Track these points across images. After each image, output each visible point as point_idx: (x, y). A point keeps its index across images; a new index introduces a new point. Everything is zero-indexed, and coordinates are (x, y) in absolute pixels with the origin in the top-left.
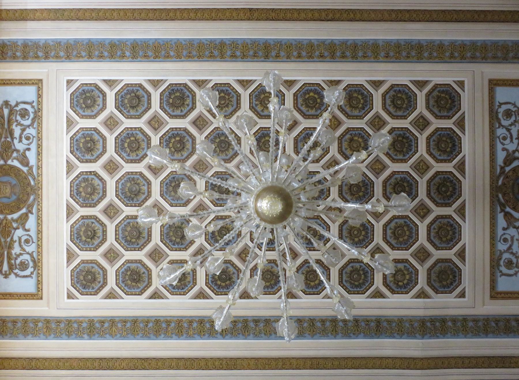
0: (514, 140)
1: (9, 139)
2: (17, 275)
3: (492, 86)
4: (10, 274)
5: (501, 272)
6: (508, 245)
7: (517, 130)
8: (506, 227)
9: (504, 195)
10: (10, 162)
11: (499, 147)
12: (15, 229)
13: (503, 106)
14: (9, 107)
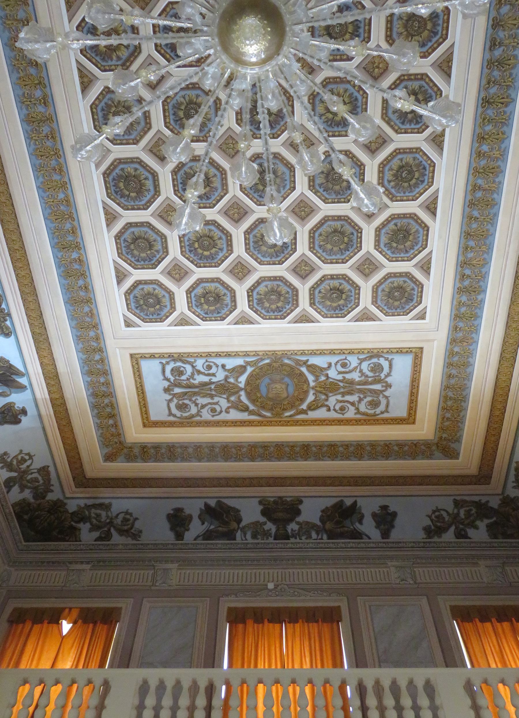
1: (213, 387)
2: (389, 375)
8: (227, 368)
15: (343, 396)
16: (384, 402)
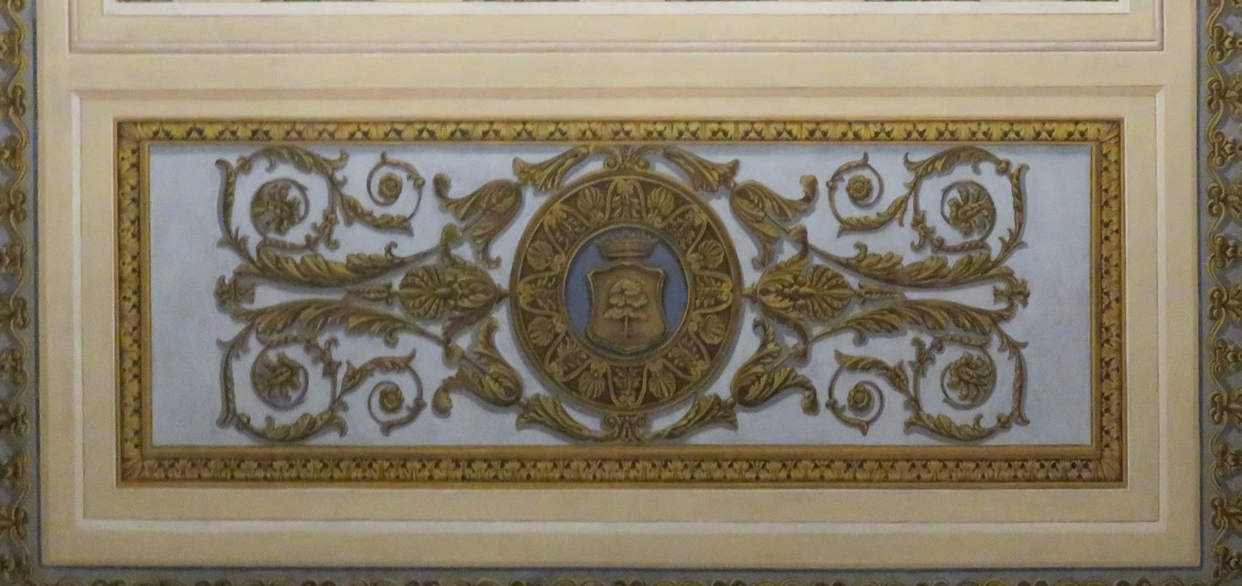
1: (396, 281)
2: (1013, 243)
4: (1008, 276)
10: (501, 278)
11: (822, 164)
15: (861, 341)
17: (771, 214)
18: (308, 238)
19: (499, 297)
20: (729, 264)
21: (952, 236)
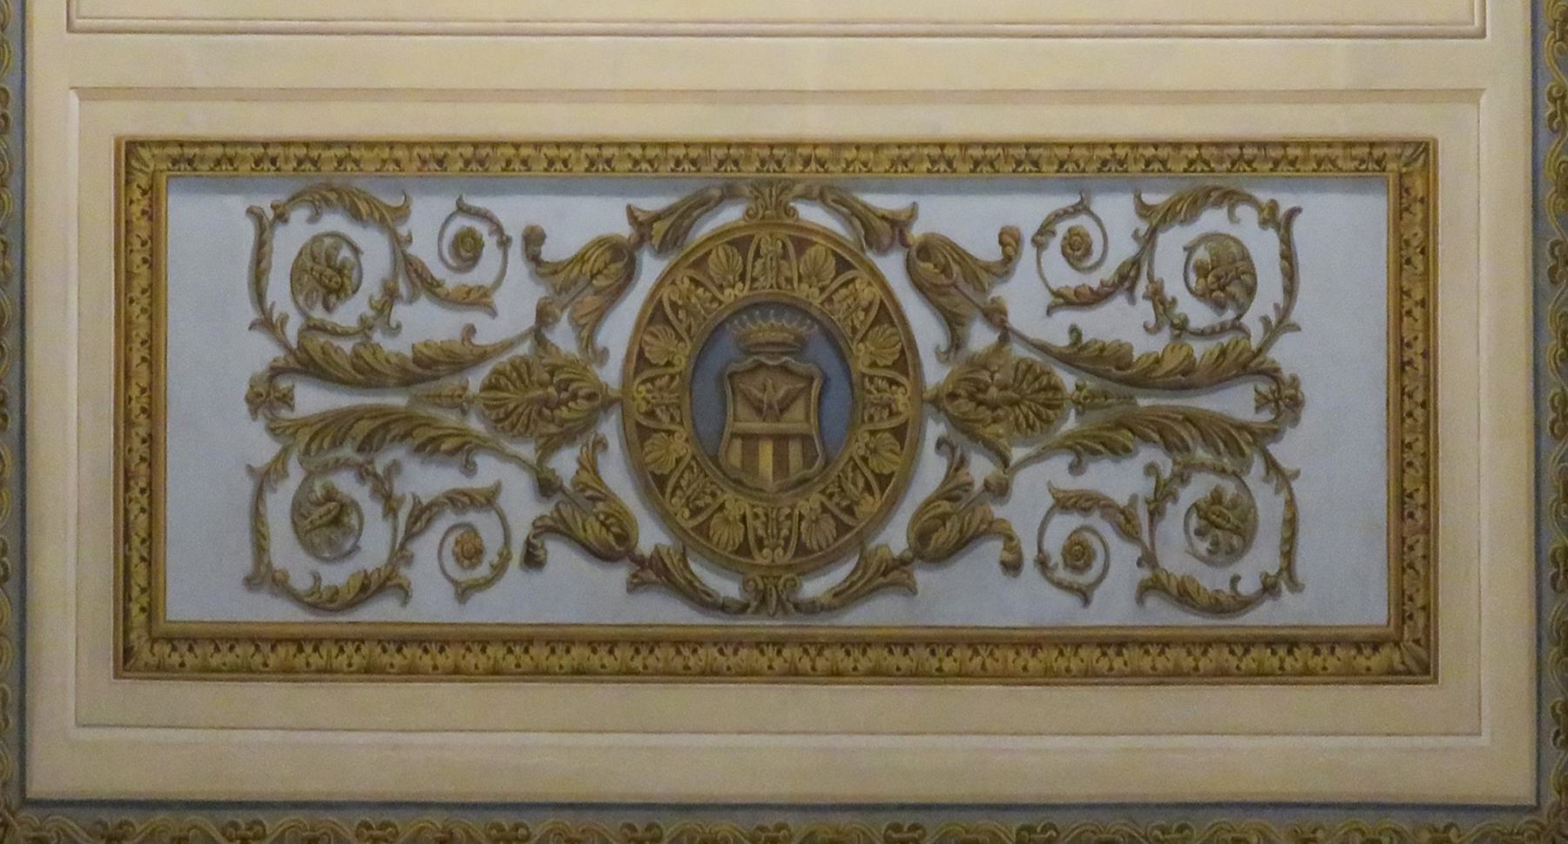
0: (1066, 317)
1: (475, 380)
2: (1281, 324)
3: (1392, 166)
4: (1272, 374)
5: (281, 217)
6: (438, 271)
7: (1125, 338)
8: (549, 253)
9: (738, 242)
10: (610, 374)
11: (1028, 210)
12: (1006, 334)
13: (1271, 237)
14: (283, 384)
15: (1076, 468)
16: (1268, 505)
17: (961, 283)
18: (362, 320)
19: (608, 404)
20: (906, 361)
21: (346, 484)
